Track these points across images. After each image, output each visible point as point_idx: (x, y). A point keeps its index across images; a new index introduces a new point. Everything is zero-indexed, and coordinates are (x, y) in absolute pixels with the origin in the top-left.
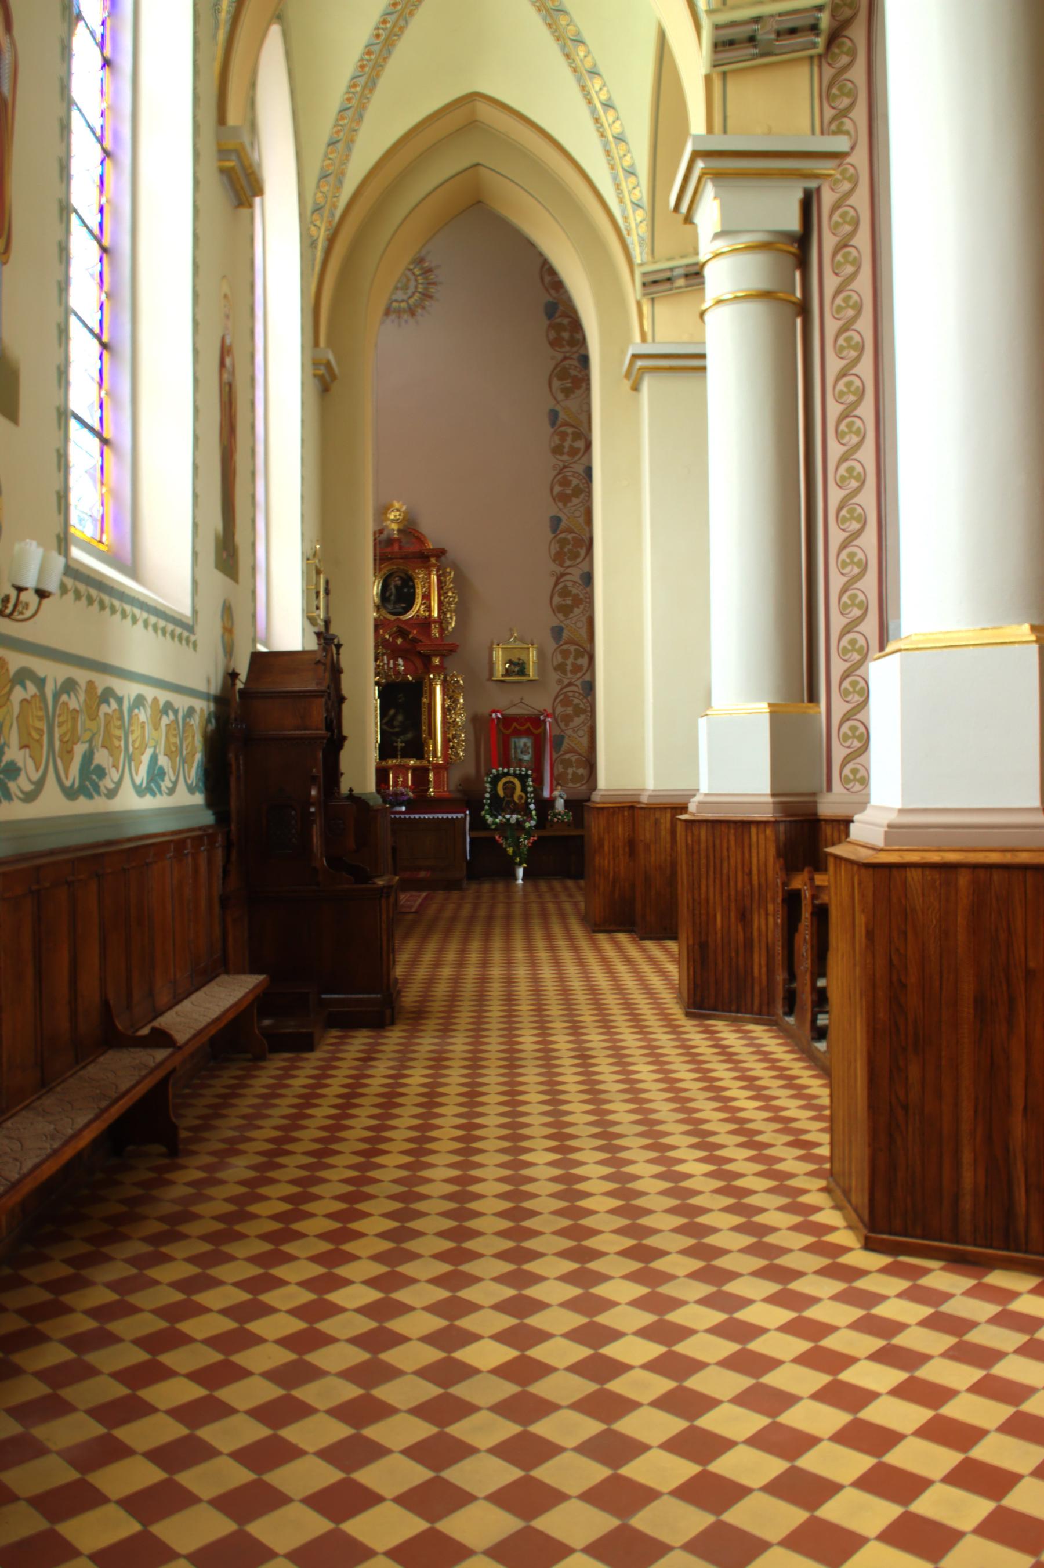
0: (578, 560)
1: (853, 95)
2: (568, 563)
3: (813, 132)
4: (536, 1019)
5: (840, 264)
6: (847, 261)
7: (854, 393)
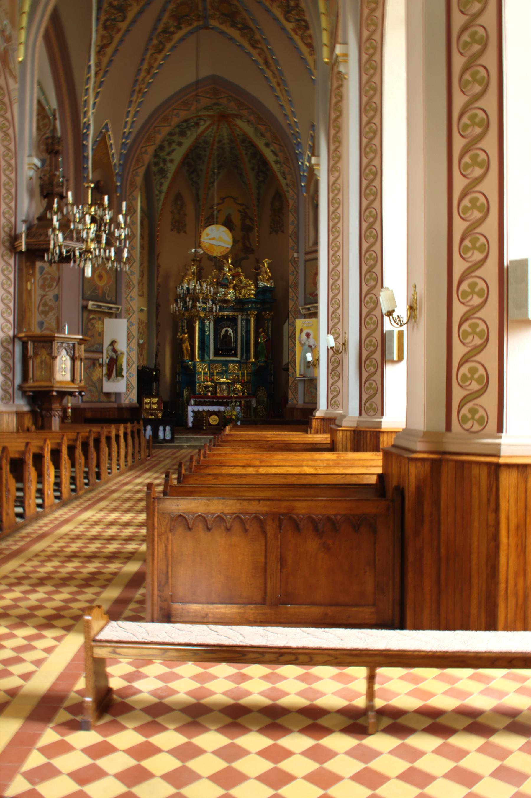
0: (53, 288)
2: (47, 290)
7: (479, 125)
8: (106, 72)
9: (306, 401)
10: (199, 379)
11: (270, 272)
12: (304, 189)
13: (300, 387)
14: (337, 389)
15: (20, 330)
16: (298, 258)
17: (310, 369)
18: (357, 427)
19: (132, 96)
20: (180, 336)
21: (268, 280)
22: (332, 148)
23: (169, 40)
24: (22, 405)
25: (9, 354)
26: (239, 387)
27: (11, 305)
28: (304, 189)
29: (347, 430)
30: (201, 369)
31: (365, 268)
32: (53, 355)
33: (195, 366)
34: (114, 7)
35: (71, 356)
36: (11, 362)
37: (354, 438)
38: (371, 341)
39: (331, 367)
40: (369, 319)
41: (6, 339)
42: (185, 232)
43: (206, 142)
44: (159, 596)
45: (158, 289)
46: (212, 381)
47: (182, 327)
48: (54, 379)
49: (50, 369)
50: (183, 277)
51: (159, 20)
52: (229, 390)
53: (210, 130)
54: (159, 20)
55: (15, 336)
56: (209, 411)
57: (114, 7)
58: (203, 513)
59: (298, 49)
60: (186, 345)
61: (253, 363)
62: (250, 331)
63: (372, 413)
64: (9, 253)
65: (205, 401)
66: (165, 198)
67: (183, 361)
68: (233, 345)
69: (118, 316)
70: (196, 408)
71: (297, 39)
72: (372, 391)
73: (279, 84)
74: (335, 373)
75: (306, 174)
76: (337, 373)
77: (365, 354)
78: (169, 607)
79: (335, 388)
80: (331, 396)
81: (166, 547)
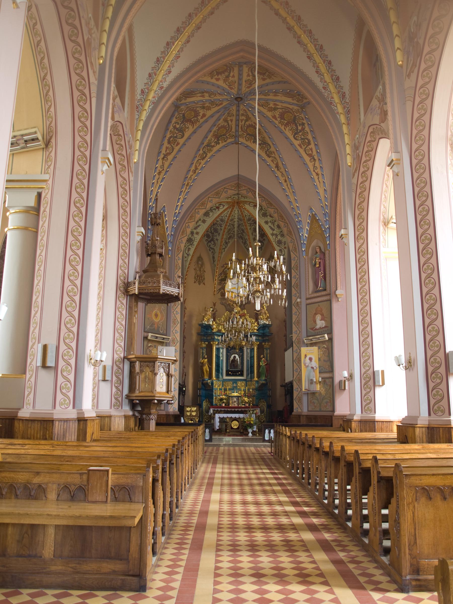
1: (51, 161)
3: (41, 173)
4: (250, 519)
5: (422, 225)
6: (425, 224)
8: (167, 171)
9: (310, 409)
10: (215, 394)
11: (268, 313)
12: (304, 253)
13: (305, 399)
14: (370, 398)
15: (129, 353)
16: (300, 302)
17: (313, 385)
18: (429, 425)
19: (182, 188)
20: (201, 360)
21: (267, 319)
22: (357, 223)
23: (210, 151)
24: (127, 410)
25: (120, 371)
26: (246, 399)
27: (123, 334)
28: (304, 253)
29: (422, 427)
30: (217, 385)
31: (426, 306)
32: (155, 372)
33: (212, 383)
34: (177, 129)
35: (167, 373)
36: (121, 377)
37: (428, 433)
38: (435, 359)
39: (363, 382)
40: (433, 343)
41: (119, 360)
42: (204, 284)
43: (222, 220)
44: (410, 554)
45: (184, 325)
46: (225, 395)
47: (203, 353)
48: (155, 390)
49: (153, 383)
50: (204, 317)
51: (206, 137)
52: (238, 402)
53: (226, 212)
54: (206, 137)
55: (124, 358)
56: (231, 417)
57: (177, 129)
58: (426, 486)
59: (301, 157)
60: (206, 368)
61: (256, 381)
62: (253, 357)
63: (440, 413)
64: (123, 296)
65: (221, 411)
66: (191, 260)
67: (203, 380)
68: (239, 368)
69: (167, 345)
70: (222, 415)
71: (302, 151)
72: (439, 397)
73: (286, 181)
74: (367, 386)
75: (305, 242)
76: (369, 386)
77: (430, 369)
78: (418, 562)
79: (368, 398)
80: (364, 404)
81: (413, 513)
